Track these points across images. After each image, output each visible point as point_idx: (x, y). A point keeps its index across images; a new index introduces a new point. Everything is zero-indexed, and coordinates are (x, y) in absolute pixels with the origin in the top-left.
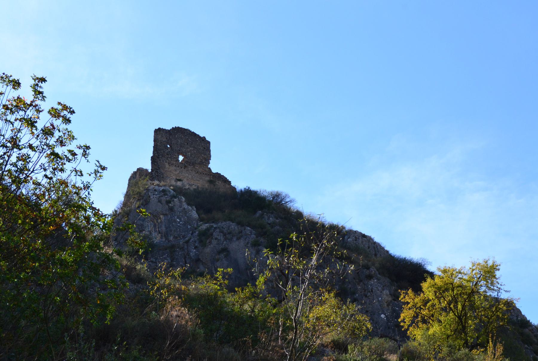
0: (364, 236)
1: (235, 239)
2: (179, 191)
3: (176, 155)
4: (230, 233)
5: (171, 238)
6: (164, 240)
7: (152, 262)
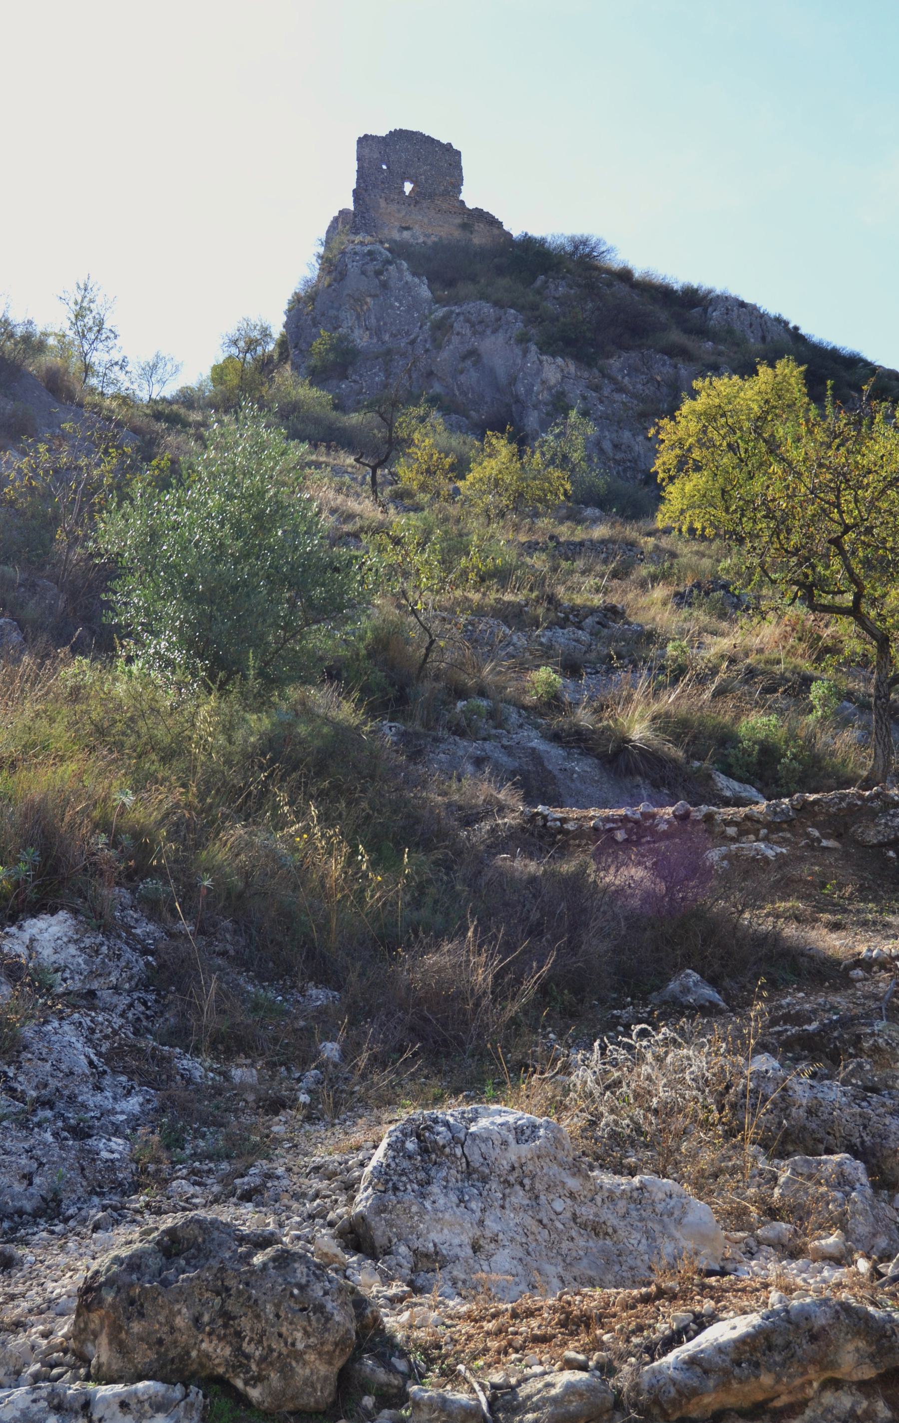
0: (742, 305)
1: (488, 332)
2: (400, 251)
3: (399, 181)
4: (481, 322)
5: (386, 337)
6: (375, 341)
7: (354, 381)
